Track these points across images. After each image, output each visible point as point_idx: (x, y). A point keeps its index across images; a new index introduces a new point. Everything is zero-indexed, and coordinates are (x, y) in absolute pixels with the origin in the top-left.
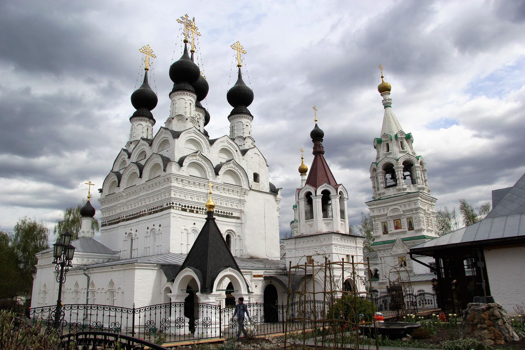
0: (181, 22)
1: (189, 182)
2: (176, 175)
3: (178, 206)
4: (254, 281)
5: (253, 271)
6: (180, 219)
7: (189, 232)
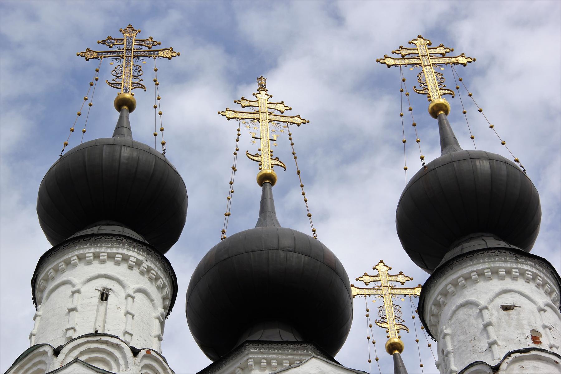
0: (100, 55)
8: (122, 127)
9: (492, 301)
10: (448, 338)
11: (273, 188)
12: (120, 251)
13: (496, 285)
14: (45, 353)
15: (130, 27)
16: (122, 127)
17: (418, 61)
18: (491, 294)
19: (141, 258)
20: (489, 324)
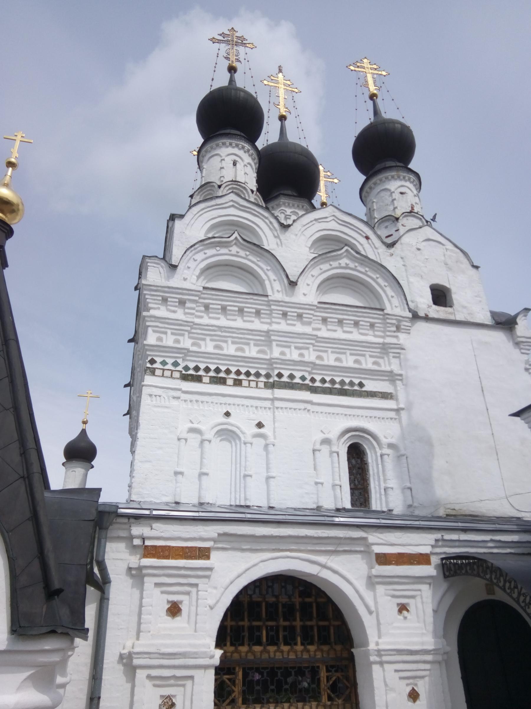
0: (219, 41)
1: (207, 307)
2: (158, 288)
3: (169, 367)
4: (387, 580)
5: (373, 537)
6: (175, 403)
7: (207, 436)
8: (232, 81)
9: (396, 189)
10: (375, 204)
11: (286, 122)
12: (241, 143)
13: (399, 183)
14: (213, 186)
15: (233, 28)
16: (232, 81)
17: (364, 70)
18: (396, 186)
19: (249, 148)
20: (395, 199)
